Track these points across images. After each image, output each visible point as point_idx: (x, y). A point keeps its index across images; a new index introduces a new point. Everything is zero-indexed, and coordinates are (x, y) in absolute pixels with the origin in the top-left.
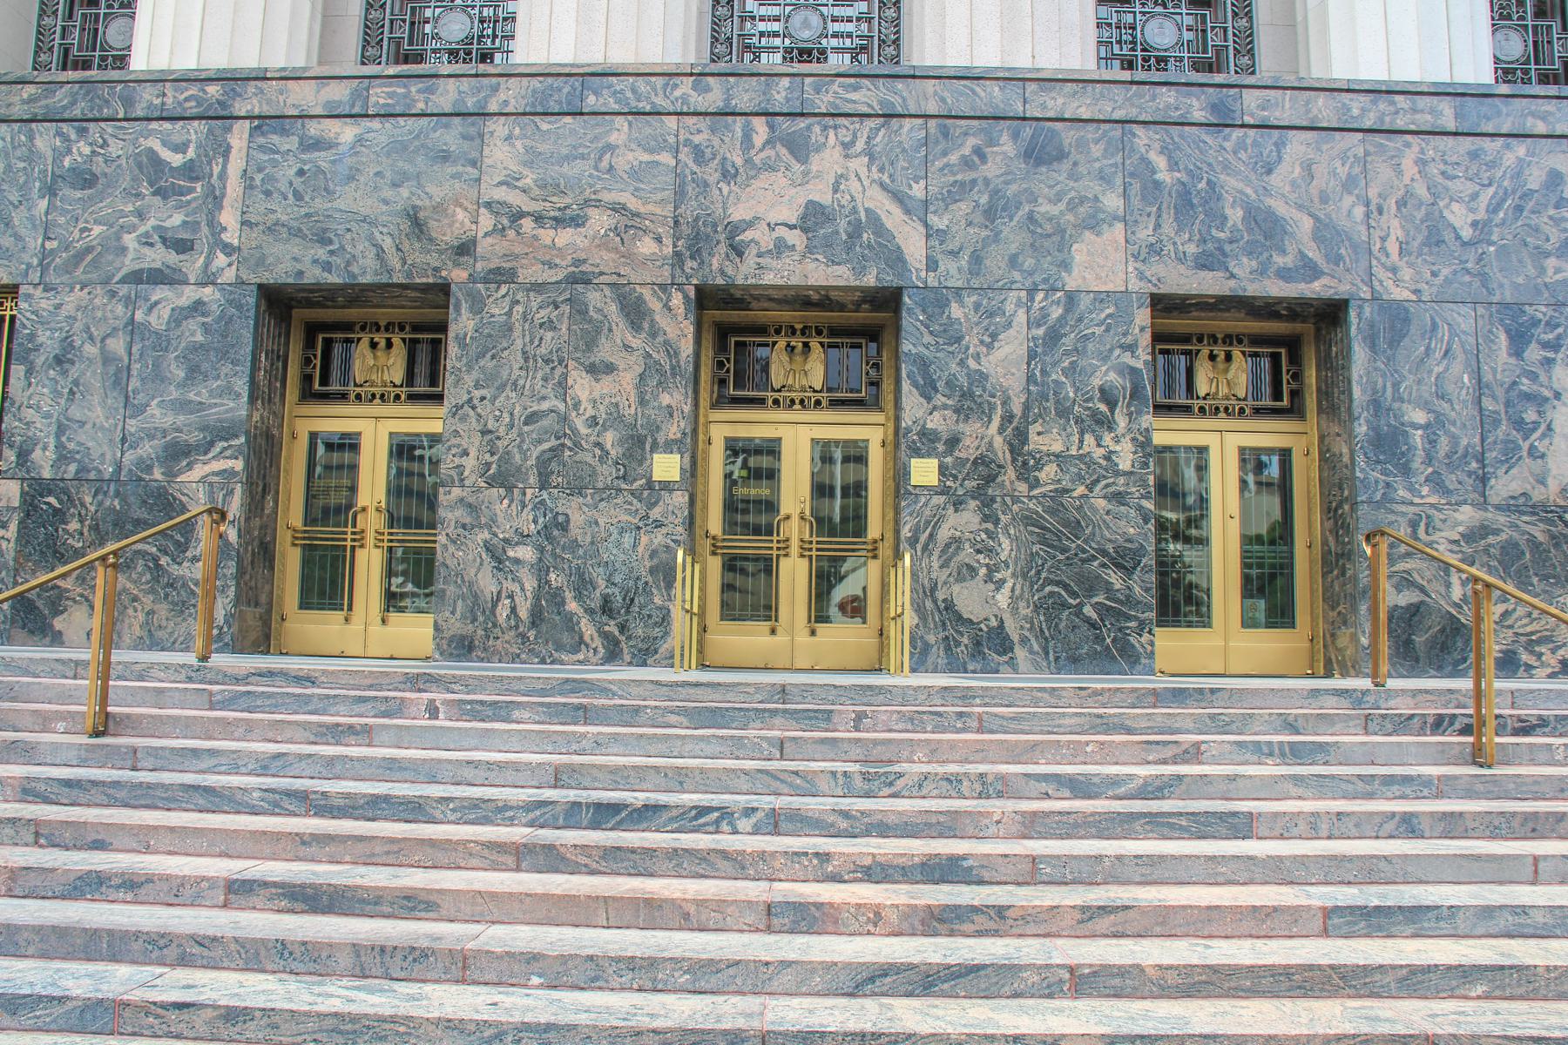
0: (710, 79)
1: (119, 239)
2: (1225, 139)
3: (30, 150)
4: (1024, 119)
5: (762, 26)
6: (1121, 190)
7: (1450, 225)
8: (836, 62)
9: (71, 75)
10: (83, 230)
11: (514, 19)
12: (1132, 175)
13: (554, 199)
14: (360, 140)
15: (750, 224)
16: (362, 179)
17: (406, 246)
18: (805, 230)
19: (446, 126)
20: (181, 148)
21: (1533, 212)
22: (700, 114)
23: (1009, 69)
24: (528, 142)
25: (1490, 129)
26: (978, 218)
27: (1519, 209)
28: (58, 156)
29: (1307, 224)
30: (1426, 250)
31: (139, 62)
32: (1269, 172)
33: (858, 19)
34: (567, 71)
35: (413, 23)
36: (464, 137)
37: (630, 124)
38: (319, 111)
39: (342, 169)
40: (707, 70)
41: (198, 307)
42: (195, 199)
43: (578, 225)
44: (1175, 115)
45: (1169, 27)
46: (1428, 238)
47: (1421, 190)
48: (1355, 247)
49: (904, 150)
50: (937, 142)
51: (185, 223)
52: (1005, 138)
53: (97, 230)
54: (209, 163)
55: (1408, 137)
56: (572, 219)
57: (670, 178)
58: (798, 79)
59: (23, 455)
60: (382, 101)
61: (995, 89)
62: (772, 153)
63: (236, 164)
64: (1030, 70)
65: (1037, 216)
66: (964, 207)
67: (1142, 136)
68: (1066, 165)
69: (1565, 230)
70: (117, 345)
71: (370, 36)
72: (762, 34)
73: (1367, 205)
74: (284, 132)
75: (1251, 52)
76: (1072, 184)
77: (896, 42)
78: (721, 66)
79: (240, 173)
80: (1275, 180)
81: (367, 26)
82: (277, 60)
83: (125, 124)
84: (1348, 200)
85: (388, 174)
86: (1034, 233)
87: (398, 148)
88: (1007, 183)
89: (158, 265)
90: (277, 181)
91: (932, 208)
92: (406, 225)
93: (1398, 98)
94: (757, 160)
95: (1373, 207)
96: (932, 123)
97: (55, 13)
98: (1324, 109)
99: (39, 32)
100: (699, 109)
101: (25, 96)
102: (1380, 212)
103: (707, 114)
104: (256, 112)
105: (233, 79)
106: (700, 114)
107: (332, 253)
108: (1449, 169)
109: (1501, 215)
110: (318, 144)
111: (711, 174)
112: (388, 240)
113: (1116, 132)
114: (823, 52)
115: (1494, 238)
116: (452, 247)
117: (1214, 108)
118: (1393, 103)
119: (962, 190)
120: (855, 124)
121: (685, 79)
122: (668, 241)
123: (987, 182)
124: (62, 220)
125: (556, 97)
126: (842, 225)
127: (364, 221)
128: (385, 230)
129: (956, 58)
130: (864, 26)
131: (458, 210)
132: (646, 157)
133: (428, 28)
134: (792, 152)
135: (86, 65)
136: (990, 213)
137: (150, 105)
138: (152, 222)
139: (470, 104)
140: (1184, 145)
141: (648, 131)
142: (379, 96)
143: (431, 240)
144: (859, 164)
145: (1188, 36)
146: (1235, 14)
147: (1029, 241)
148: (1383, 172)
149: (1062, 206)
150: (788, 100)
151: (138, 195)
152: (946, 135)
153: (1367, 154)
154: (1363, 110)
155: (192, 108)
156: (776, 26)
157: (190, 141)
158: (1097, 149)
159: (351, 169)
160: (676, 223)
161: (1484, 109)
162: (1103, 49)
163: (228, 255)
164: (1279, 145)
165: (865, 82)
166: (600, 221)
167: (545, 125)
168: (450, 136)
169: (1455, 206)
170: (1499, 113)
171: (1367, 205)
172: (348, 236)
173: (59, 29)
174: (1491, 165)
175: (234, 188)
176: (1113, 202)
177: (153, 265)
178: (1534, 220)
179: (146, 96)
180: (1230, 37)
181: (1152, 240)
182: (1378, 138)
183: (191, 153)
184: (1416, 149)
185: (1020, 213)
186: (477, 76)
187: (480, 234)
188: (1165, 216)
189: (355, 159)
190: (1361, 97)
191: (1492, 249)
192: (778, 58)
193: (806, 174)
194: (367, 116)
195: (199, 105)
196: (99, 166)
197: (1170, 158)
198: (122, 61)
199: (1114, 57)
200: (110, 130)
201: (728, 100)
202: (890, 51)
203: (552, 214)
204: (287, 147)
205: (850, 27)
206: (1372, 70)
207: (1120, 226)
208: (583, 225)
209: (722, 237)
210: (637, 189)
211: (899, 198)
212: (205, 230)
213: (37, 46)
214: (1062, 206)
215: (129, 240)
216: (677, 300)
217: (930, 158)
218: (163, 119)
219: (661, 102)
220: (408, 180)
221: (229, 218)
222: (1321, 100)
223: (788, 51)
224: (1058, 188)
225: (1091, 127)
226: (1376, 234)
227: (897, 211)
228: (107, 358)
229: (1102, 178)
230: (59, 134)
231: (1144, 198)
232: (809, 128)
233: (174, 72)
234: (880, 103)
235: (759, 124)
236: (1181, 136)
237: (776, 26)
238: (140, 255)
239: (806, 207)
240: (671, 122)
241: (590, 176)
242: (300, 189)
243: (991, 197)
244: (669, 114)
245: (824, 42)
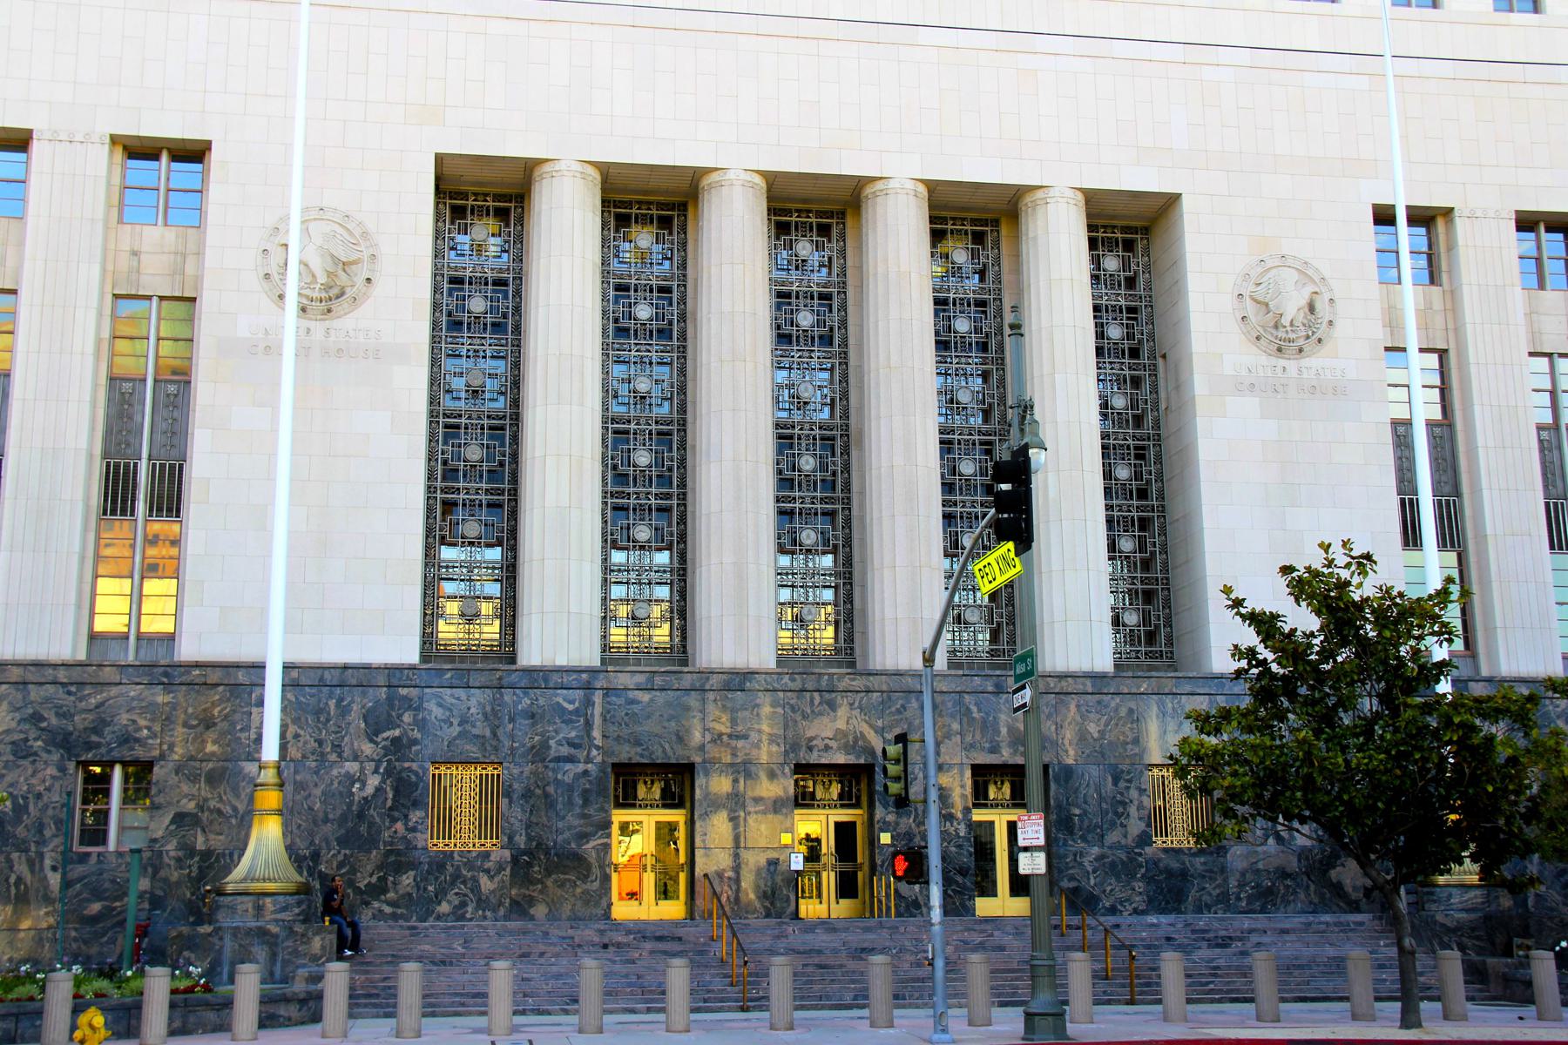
14: (652, 700)
20: (571, 702)
41: (586, 772)
59: (510, 838)
63: (598, 710)
70: (551, 789)
74: (618, 696)
110: (633, 702)
117: (997, 685)
142: (658, 681)
155: (575, 684)
175: (597, 721)
176: (956, 726)
215: (552, 743)
216: (787, 770)
221: (596, 733)
228: (546, 795)
235: (816, 695)
238: (555, 749)
240: (781, 694)
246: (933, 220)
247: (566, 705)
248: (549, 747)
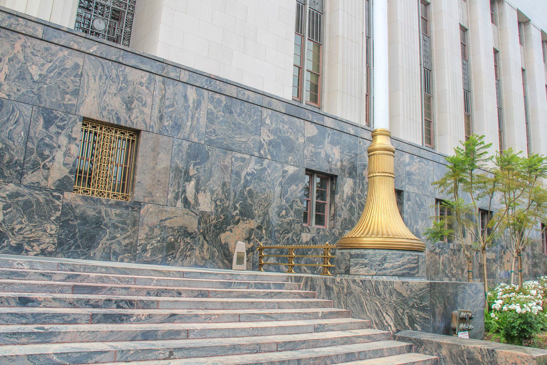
21: (65, 76)
30: (17, 80)
46: (19, 76)
47: (21, 57)
55: (21, 36)
93: (20, 19)
108: (35, 52)
109: (52, 74)
115: (47, 82)
118: (18, 21)
161: (55, 34)
169: (34, 66)
170: (61, 37)
174: (53, 55)
178: (65, 79)
180: (123, 33)
182: (7, 32)
191: (45, 86)
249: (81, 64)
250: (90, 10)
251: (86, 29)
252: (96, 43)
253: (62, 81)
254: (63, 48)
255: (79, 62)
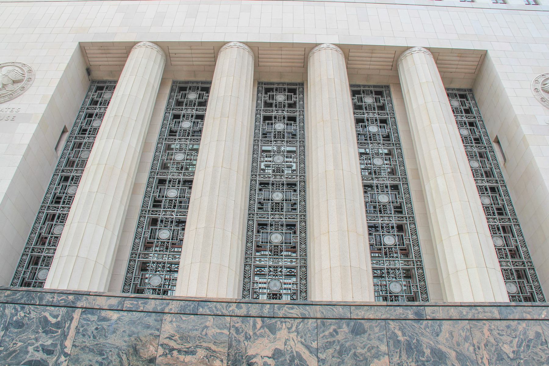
0: (242, 304)
1: (27, 347)
2: (421, 324)
3: (3, 313)
4: (351, 319)
5: (260, 285)
6: (386, 344)
7: (505, 353)
8: (286, 299)
9: (24, 288)
10: (14, 344)
11: (176, 280)
12: (390, 338)
13: (185, 344)
14: (119, 319)
15: (255, 356)
16: (118, 333)
17: (131, 358)
18: (274, 359)
19: (150, 316)
20: (56, 317)
21: (534, 347)
22: (238, 316)
23: (345, 302)
24: (178, 324)
25: (511, 317)
26: (336, 355)
27: (528, 346)
28: (12, 315)
29: (453, 354)
30: (498, 362)
31: (47, 286)
32: (438, 335)
33: (293, 284)
34: (193, 299)
35: (142, 279)
36: (156, 320)
37: (214, 319)
38: (106, 307)
39: (111, 329)
40: (241, 301)
42: (57, 335)
43: (193, 354)
44: (403, 317)
45: (398, 285)
46: (498, 357)
47: (492, 340)
48: (472, 362)
49: (309, 330)
50: (321, 328)
51: (52, 344)
52: (344, 326)
53: (20, 344)
54: (65, 323)
55: (484, 321)
56: (191, 352)
57: (227, 339)
58: (272, 305)
60: (128, 306)
61: (340, 308)
62: (263, 331)
63: (74, 324)
64: (352, 302)
65: (357, 354)
66: (331, 351)
67: (392, 324)
68: (366, 335)
69: (547, 354)
71: (127, 282)
72: (260, 288)
73: (474, 346)
74: (93, 314)
75: (426, 293)
76: (369, 342)
77: (306, 292)
78: (247, 300)
79: (75, 327)
80: (440, 338)
81: (126, 279)
82: (94, 289)
83: (38, 307)
84: (467, 345)
85: (127, 332)
86: (356, 360)
87: (132, 323)
88: (346, 342)
89: (39, 359)
90: (88, 331)
91: (319, 351)
92: (131, 351)
93: (478, 308)
94: (258, 333)
95: (476, 347)
96: (319, 321)
97: (23, 266)
98: (454, 313)
99: (16, 272)
100: (238, 315)
101: (6, 294)
102: (479, 349)
103: (240, 316)
104: (84, 306)
105: (78, 294)
106: (238, 316)
107: (103, 359)
108: (500, 332)
109: (522, 348)
110: (105, 319)
111: (241, 338)
112: (125, 356)
113: (383, 323)
114: (281, 295)
115: (522, 357)
116: (147, 360)
117: (416, 314)
118: (477, 310)
119: (329, 345)
120: (292, 321)
121: (233, 304)
122: (225, 362)
123: (339, 341)
124: (7, 340)
125: (189, 308)
126: (288, 357)
127: (117, 348)
128: (124, 352)
129: (326, 298)
130: (295, 286)
131: (151, 346)
132: (219, 331)
133: (147, 281)
134: (270, 331)
135: (29, 285)
136: (340, 353)
137: (48, 301)
138: (40, 343)
139: (159, 309)
140: (407, 327)
141: (220, 322)
142: (128, 304)
143: (140, 357)
144: (293, 335)
145: (404, 288)
146: (420, 280)
147: (355, 363)
148: (477, 334)
149: (366, 350)
150: (269, 312)
151: (37, 332)
152: (324, 325)
153: (471, 328)
154: (467, 312)
155: (62, 303)
156: (265, 286)
157: (60, 314)
158: (376, 330)
159: (114, 329)
160: (228, 355)
161: (508, 311)
162: (376, 293)
163: (66, 357)
164: (440, 326)
165: (296, 306)
166: (201, 353)
167: (184, 317)
168: (151, 320)
169: (505, 346)
170: (513, 312)
171: (474, 346)
172: (110, 353)
173: (23, 272)
174: (515, 330)
175: (72, 332)
176: (383, 348)
177: (37, 359)
178: (535, 350)
179: (48, 298)
180: (419, 288)
181: (399, 361)
182: (474, 322)
183: (59, 319)
184: (487, 325)
185: (351, 353)
186: (162, 299)
187: (158, 356)
188: (402, 353)
189: (116, 325)
190: (466, 308)
191: (522, 361)
192: (265, 297)
193: (275, 338)
194: (122, 310)
195: (65, 302)
196: (26, 320)
197: (402, 332)
198: (41, 284)
199: (380, 296)
200: (32, 308)
201: (248, 312)
202: (304, 294)
203: (184, 350)
204: (93, 319)
205: (290, 286)
206: (468, 299)
207: (387, 357)
208: (195, 354)
209: (245, 361)
210: (215, 342)
211: (308, 347)
212: (59, 347)
213: (14, 277)
214: (366, 350)
215: (30, 349)
217: (318, 333)
218: (51, 306)
219: (225, 312)
220: (134, 334)
221: (68, 343)
222: (452, 309)
223: (269, 294)
224: (364, 343)
225: (374, 321)
226: (479, 357)
227: (307, 352)
229: (379, 339)
230: (15, 308)
231: (394, 346)
232: (276, 322)
233: (58, 290)
234: (301, 314)
235: (259, 320)
236: (406, 324)
237: (265, 286)
239: (275, 350)
240: (228, 319)
241: (199, 337)
242: (96, 335)
243: (340, 347)
244: (228, 316)
245: (281, 291)
246: (351, 86)
247: (50, 319)
248: (27, 352)
249: (541, 331)
250: (383, 277)
251: (388, 297)
252: (543, 308)
253: (533, 352)
254: (519, 321)
255: (538, 330)
